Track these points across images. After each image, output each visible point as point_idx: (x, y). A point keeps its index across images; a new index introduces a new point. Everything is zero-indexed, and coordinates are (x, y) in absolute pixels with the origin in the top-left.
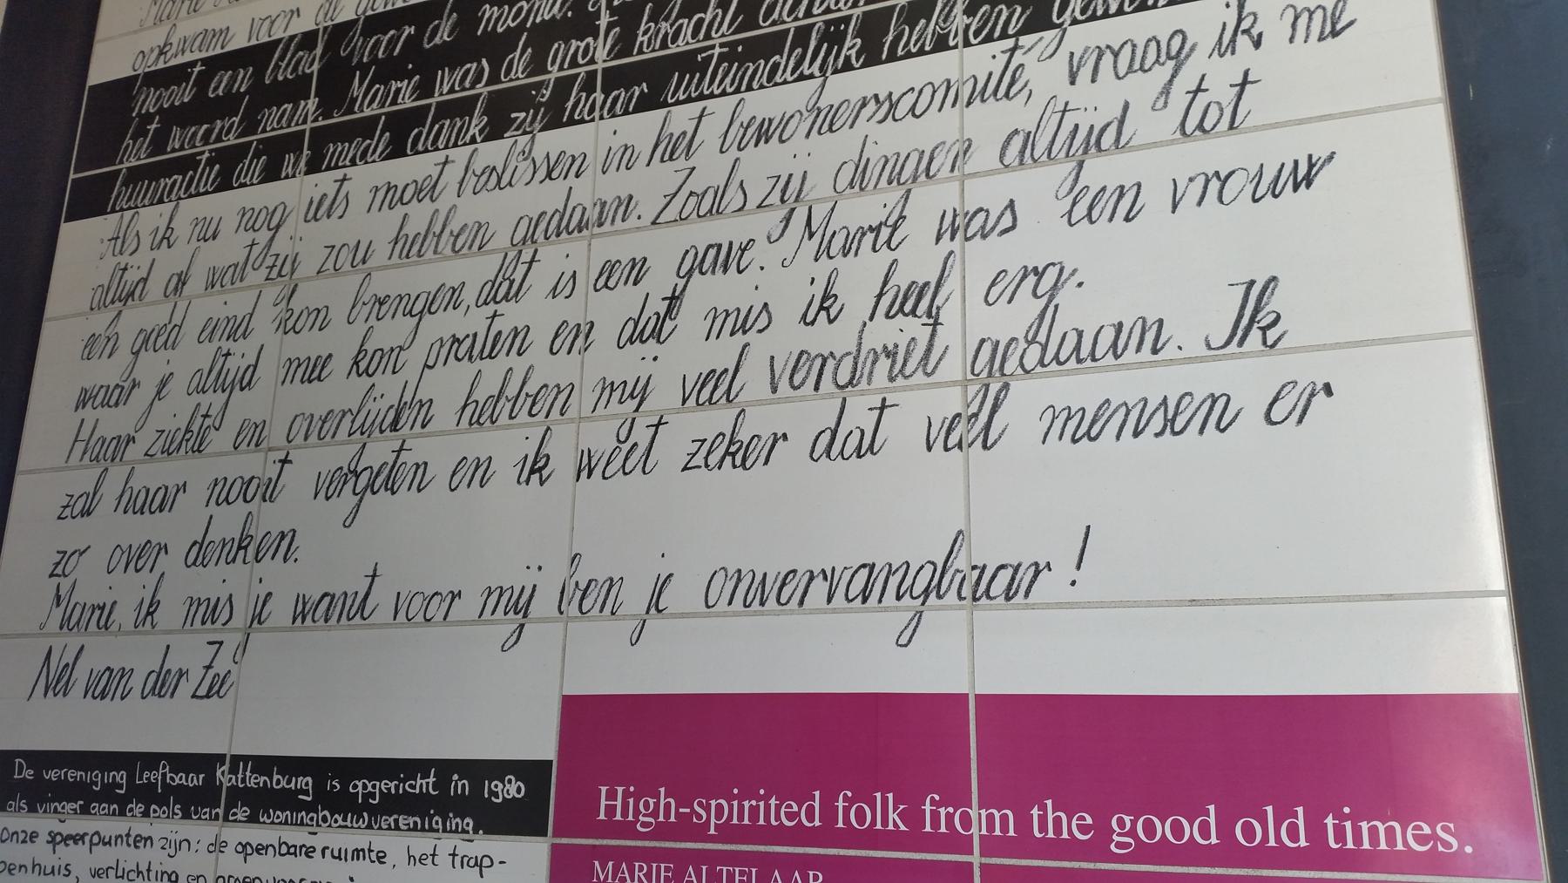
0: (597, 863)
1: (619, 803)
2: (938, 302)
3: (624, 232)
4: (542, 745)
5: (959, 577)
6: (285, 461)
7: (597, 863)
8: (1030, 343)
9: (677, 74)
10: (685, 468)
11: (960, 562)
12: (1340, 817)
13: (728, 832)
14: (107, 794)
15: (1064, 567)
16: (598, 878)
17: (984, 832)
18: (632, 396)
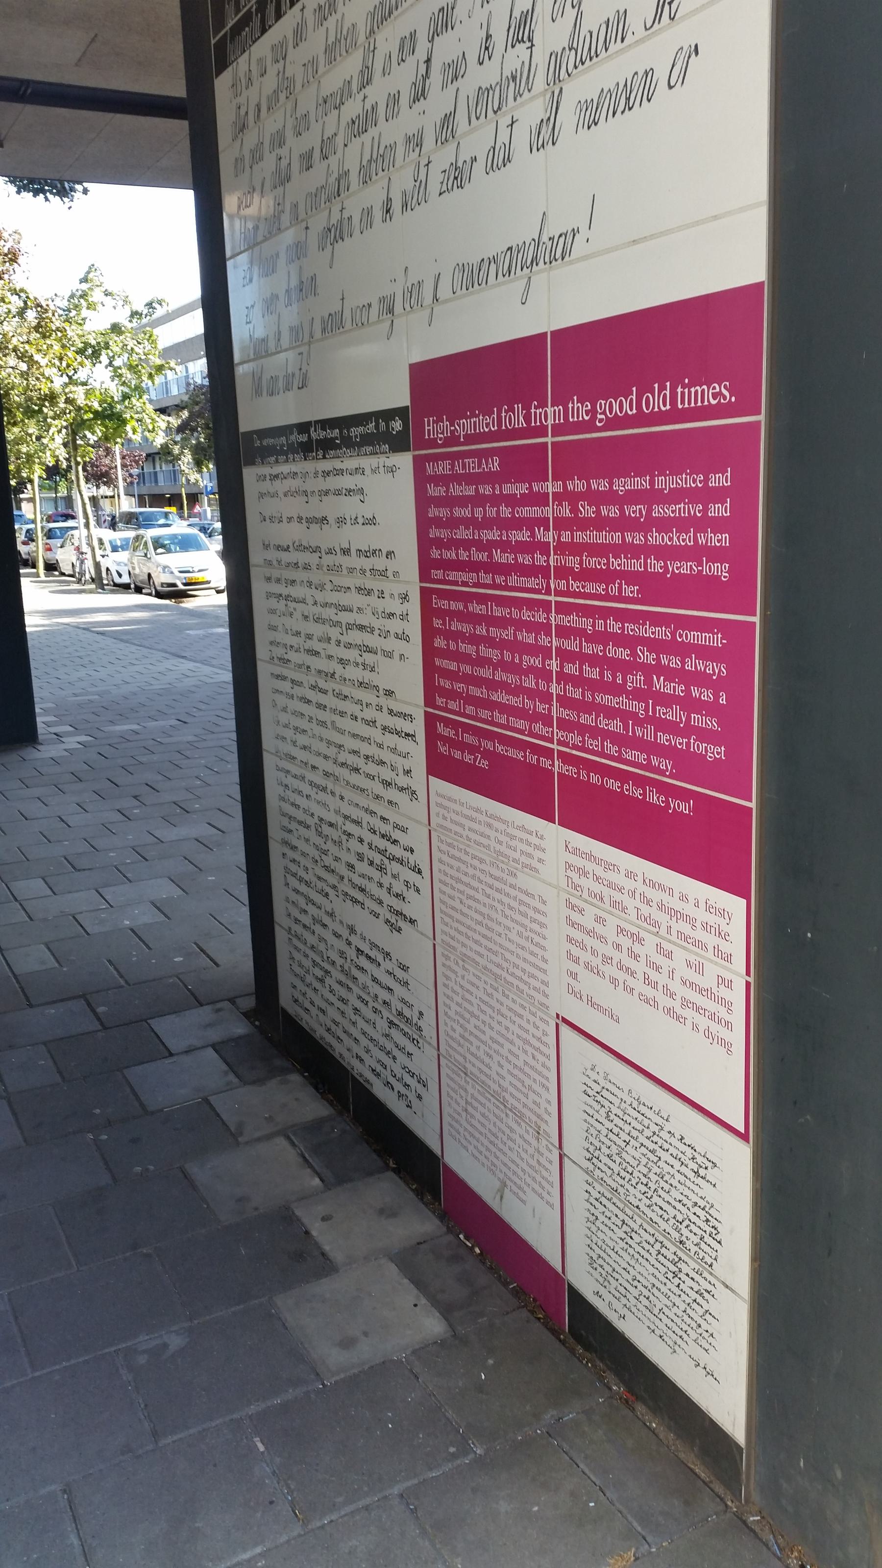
0: (655, 677)
1: (431, 428)
2: (532, 27)
3: (407, 9)
4: (401, 397)
5: (544, 246)
6: (307, 228)
7: (655, 677)
8: (570, 50)
9: (182, 959)
10: (440, 194)
11: (545, 238)
12: (683, 387)
13: (471, 439)
14: (282, 452)
15: (584, 228)
16: (656, 688)
17: (553, 422)
18: (417, 145)
